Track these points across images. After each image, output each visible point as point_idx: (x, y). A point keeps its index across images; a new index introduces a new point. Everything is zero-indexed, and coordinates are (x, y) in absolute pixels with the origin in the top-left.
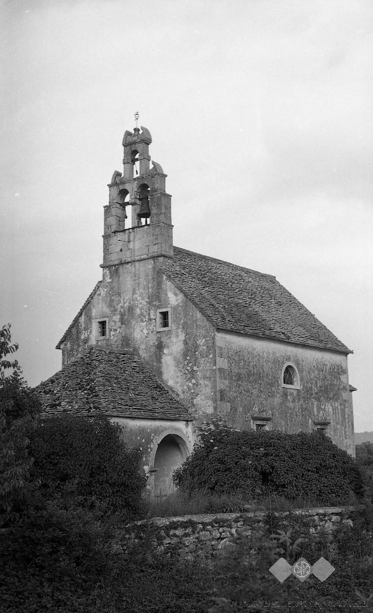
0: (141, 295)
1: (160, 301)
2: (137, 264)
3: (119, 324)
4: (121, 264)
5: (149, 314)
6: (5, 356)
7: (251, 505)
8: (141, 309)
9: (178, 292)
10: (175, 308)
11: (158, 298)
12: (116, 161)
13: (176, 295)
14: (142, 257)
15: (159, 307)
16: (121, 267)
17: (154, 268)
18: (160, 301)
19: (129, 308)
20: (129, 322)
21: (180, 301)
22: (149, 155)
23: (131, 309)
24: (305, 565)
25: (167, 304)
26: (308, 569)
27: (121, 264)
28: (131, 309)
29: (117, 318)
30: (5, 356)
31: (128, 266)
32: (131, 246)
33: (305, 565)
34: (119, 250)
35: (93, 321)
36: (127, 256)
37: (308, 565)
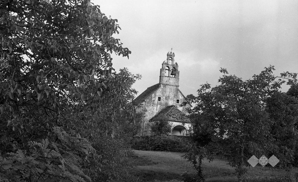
0: (172, 94)
1: (177, 97)
2: (171, 86)
3: (165, 99)
4: (167, 85)
5: (174, 99)
6: (126, 53)
7: (67, 126)
8: (172, 97)
9: (182, 96)
10: (181, 100)
11: (177, 96)
12: (165, 58)
13: (182, 97)
14: (174, 85)
15: (177, 98)
16: (166, 85)
17: (176, 89)
18: (177, 97)
19: (168, 96)
20: (168, 99)
21: (182, 98)
22: (147, 89)
23: (169, 97)
24: (265, 159)
25: (179, 98)
26: (266, 161)
27: (167, 85)
28: (169, 97)
29: (164, 98)
30: (126, 53)
31: (169, 86)
32: (170, 81)
33: (265, 159)
34: (166, 81)
35: (157, 96)
36: (168, 83)
37: (266, 159)
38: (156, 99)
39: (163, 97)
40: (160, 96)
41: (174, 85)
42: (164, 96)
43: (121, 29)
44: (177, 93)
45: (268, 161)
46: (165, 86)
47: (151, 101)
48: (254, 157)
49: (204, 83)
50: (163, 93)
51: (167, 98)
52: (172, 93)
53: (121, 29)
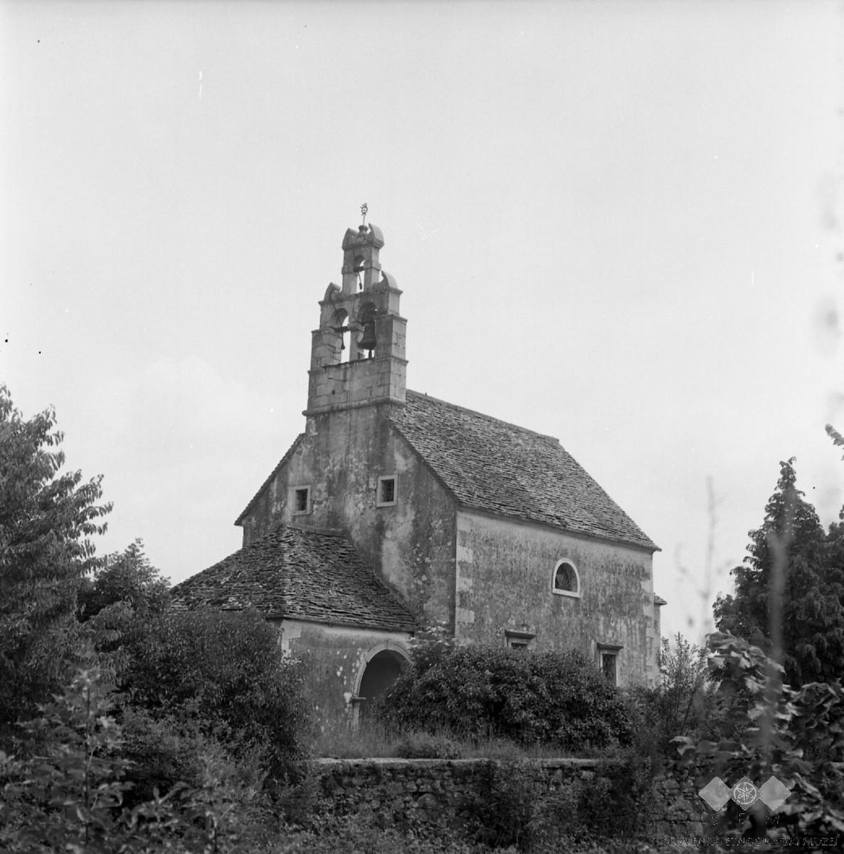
0: (358, 455)
2: (354, 412)
5: (368, 483)
8: (356, 475)
9: (408, 453)
15: (381, 473)
17: (377, 419)
21: (410, 466)
26: (753, 793)
28: (343, 475)
29: (322, 486)
34: (329, 391)
36: (340, 401)
38: (285, 504)
39: (319, 486)
40: (303, 484)
41: (365, 402)
42: (321, 475)
43: (829, 429)
44: (383, 442)
45: (758, 796)
46: (326, 421)
47: (268, 523)
48: (718, 782)
49: (825, 433)
50: (317, 462)
51: (335, 486)
52: (358, 449)
53: (829, 429)
